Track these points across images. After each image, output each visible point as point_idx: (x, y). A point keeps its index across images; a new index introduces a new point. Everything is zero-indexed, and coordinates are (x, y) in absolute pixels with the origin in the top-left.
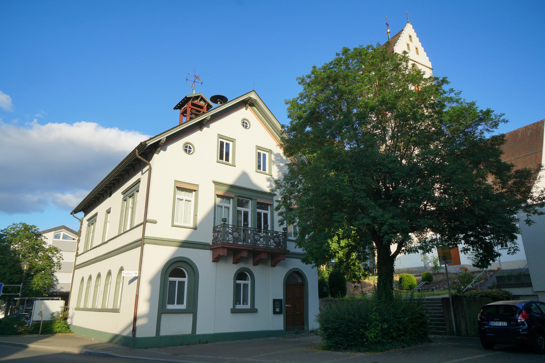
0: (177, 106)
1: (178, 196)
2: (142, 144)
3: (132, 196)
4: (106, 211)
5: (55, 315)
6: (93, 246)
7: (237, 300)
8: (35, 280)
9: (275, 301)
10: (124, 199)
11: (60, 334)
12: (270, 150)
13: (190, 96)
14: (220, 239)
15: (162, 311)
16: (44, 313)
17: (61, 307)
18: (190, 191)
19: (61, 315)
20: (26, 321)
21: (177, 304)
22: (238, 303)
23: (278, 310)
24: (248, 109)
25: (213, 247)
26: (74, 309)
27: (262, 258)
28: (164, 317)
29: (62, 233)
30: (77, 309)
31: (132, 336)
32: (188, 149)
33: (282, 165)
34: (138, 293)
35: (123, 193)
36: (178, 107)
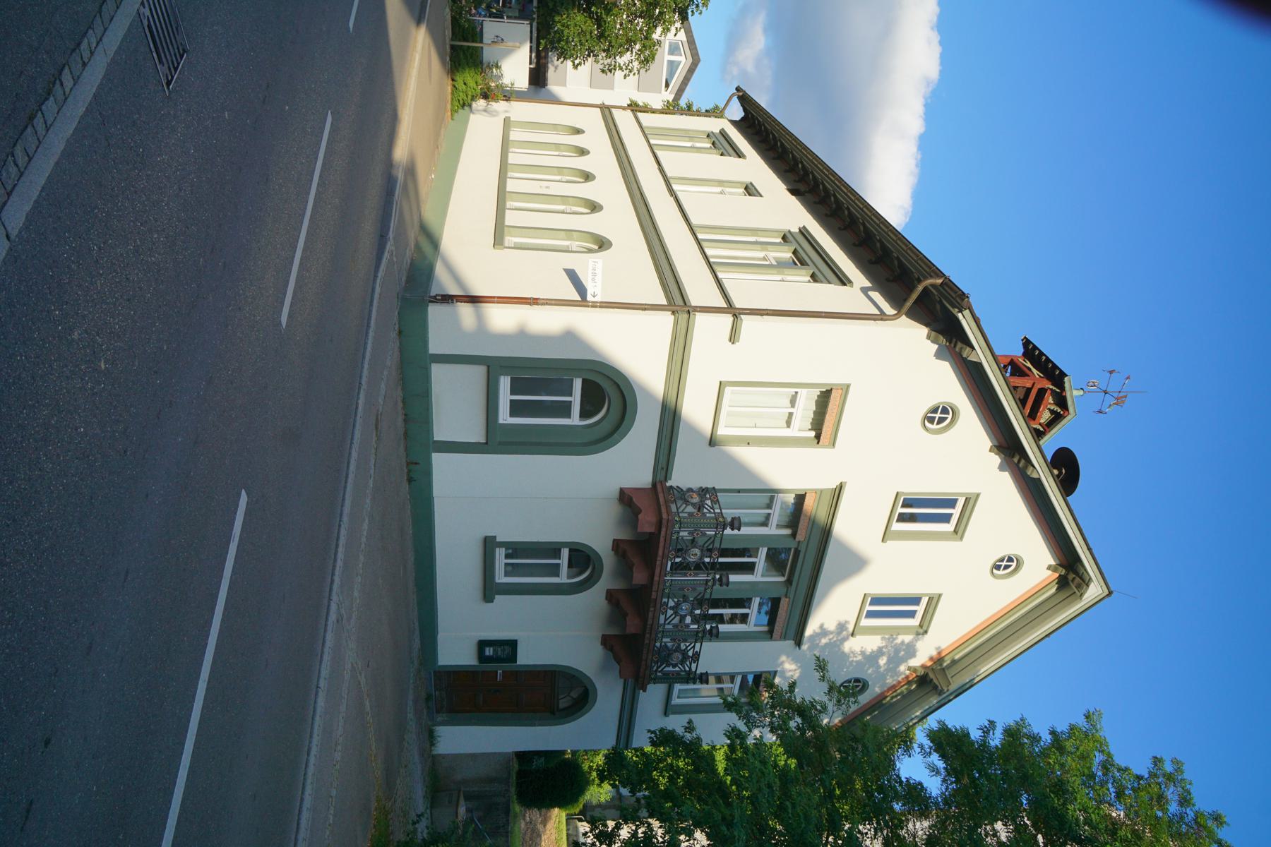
0: (1035, 347)
1: (803, 393)
2: (963, 300)
3: (799, 260)
4: (751, 183)
5: (494, 70)
6: (659, 153)
7: (515, 549)
8: (578, 18)
9: (513, 644)
10: (711, 135)
11: (449, 88)
12: (926, 632)
13: (1067, 385)
14: (682, 512)
15: (494, 367)
16: (501, 47)
17: (512, 84)
18: (818, 424)
19: (493, 84)
20: (484, 6)
21: (511, 401)
22: (510, 551)
23: (489, 651)
24: (1050, 572)
25: (660, 491)
26: (507, 115)
27: (627, 619)
28: (477, 374)
29: (682, 59)
30: (507, 123)
31: (433, 294)
32: (939, 416)
33: (883, 661)
34: (542, 304)
35: (804, 232)
36: (1030, 349)
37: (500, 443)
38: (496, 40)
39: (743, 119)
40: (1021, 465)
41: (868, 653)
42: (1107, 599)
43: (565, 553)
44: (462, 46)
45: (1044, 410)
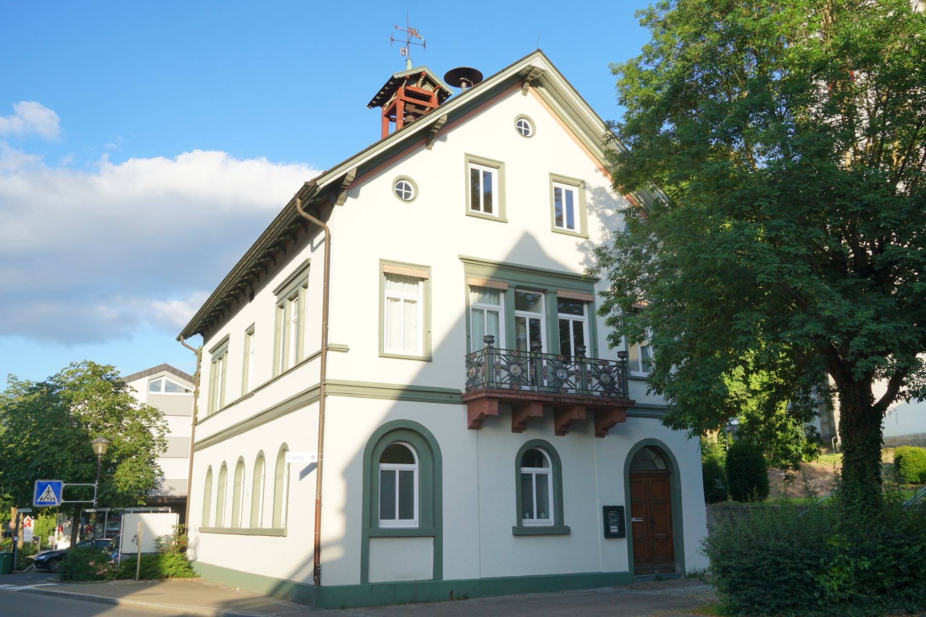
0: (375, 99)
1: (388, 293)
2: (309, 186)
4: (246, 330)
5: (162, 542)
6: (226, 404)
7: (524, 509)
8: (120, 473)
9: (607, 510)
10: (213, 361)
11: (174, 579)
12: (582, 182)
13: (401, 76)
14: (482, 381)
16: (141, 537)
17: (174, 527)
18: (414, 280)
20: (110, 553)
22: (527, 514)
23: (614, 529)
24: (529, 93)
25: (467, 399)
26: (198, 530)
28: (376, 546)
29: (163, 379)
30: (203, 530)
31: (313, 583)
32: (403, 190)
33: (610, 212)
35: (278, 292)
36: (378, 101)
37: (434, 526)
38: (136, 542)
39: (203, 335)
40: (439, 127)
41: (603, 225)
42: (544, 52)
43: (526, 470)
44: (140, 570)
45: (422, 90)
